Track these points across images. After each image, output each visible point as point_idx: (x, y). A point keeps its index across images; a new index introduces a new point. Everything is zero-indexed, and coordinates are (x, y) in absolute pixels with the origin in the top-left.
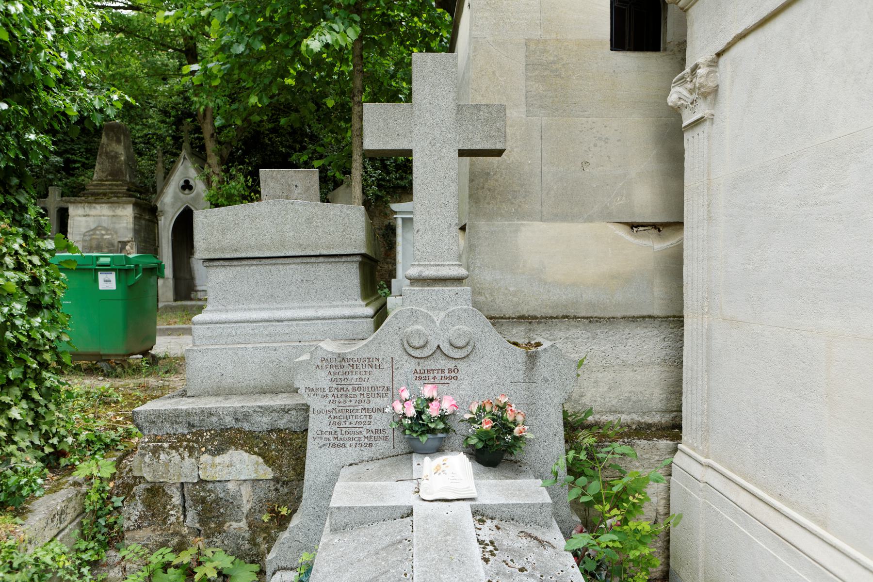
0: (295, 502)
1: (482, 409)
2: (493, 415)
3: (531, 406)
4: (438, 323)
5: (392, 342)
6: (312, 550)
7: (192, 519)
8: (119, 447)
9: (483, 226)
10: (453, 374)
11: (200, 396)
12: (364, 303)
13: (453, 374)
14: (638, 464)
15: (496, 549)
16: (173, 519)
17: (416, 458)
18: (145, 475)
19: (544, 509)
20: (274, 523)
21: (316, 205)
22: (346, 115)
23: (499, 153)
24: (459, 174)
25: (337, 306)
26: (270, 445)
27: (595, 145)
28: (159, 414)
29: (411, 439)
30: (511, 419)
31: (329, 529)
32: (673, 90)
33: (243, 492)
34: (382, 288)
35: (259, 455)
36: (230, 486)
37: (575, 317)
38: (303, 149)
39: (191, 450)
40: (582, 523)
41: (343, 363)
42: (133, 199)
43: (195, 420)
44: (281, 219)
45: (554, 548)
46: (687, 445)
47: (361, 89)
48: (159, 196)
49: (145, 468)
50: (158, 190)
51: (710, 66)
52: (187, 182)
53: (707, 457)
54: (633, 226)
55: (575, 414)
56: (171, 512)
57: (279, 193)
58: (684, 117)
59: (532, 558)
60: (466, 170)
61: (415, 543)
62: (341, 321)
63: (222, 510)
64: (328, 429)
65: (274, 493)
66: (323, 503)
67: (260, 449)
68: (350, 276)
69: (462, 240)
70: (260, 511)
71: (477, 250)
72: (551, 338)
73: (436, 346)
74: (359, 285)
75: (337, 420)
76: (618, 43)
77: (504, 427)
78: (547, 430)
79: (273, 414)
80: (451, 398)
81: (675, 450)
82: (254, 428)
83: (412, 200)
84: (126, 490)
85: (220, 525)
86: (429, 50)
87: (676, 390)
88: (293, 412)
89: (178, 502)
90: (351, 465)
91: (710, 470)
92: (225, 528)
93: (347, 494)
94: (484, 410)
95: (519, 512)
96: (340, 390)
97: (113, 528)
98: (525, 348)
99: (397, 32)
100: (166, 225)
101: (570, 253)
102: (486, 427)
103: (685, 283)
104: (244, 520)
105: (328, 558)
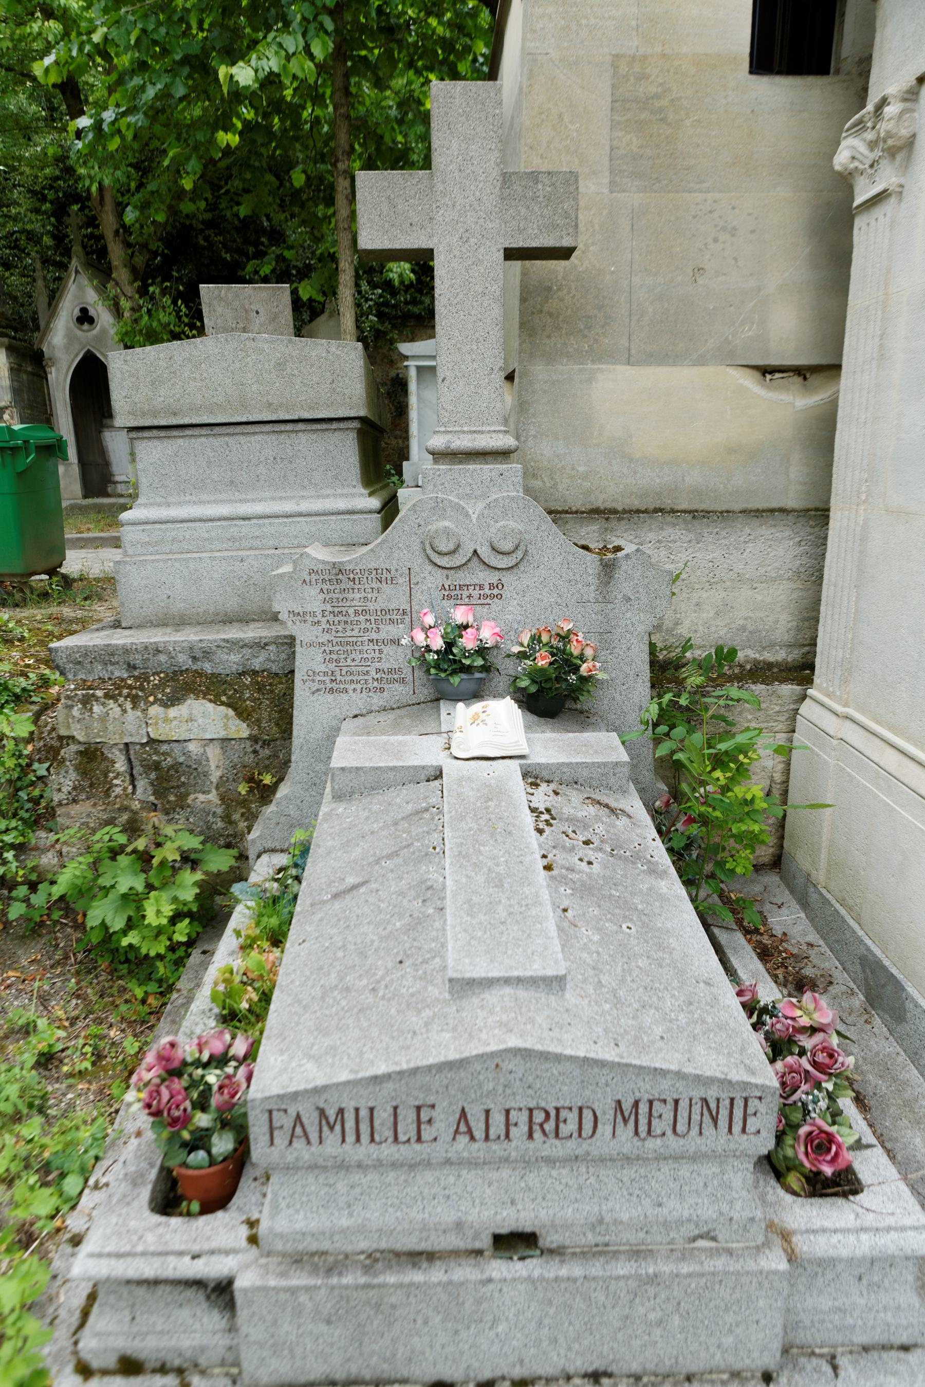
0: (282, 768)
1: (536, 639)
2: (552, 647)
3: (605, 638)
4: (474, 518)
5: (408, 546)
6: (309, 827)
7: (144, 790)
8: (34, 699)
9: (540, 371)
10: (496, 592)
11: (140, 627)
12: (366, 492)
13: (496, 592)
14: (750, 717)
15: (554, 819)
16: (118, 790)
17: (444, 706)
18: (75, 733)
19: (618, 770)
20: (254, 795)
21: (290, 341)
22: (325, 196)
23: (565, 253)
24: (504, 289)
25: (328, 496)
26: (242, 693)
27: (716, 240)
28: (86, 652)
29: (438, 680)
30: (576, 652)
31: (330, 797)
32: (844, 144)
33: (210, 755)
34: (389, 475)
35: (228, 705)
36: (192, 747)
37: (673, 511)
38: (260, 255)
39: (135, 700)
40: (670, 792)
41: (340, 576)
42: (6, 340)
43: (137, 659)
44: (238, 365)
45: (629, 816)
46: (819, 690)
47: (347, 148)
48: (44, 334)
49: (74, 723)
50: (42, 324)
51: (905, 100)
52: (84, 311)
53: (846, 705)
54: (765, 371)
55: (666, 648)
56: (115, 782)
57: (231, 323)
58: (857, 189)
59: (600, 829)
60: (516, 282)
61: (446, 809)
62: (334, 517)
63: (183, 779)
64: (323, 668)
65: (252, 756)
66: (320, 767)
67: (229, 698)
68: (345, 450)
69: (508, 397)
70: (234, 780)
71: (532, 410)
72: (636, 540)
73: (472, 550)
74: (358, 465)
75: (334, 657)
76: (767, 57)
77: (566, 663)
78: (627, 669)
79: (244, 651)
80: (493, 623)
81: (804, 697)
82: (219, 670)
83: (433, 336)
84: (51, 754)
85: (183, 797)
86: (455, 76)
87: (810, 616)
88: (272, 648)
89: (123, 769)
90: (356, 716)
91: (848, 723)
92: (189, 801)
93: (349, 751)
94: (540, 641)
95: (585, 773)
96: (337, 613)
97: (38, 804)
98: (599, 554)
99: (400, 43)
100: (60, 380)
101: (670, 412)
102: (541, 663)
103: (836, 459)
104: (214, 791)
105: (331, 831)
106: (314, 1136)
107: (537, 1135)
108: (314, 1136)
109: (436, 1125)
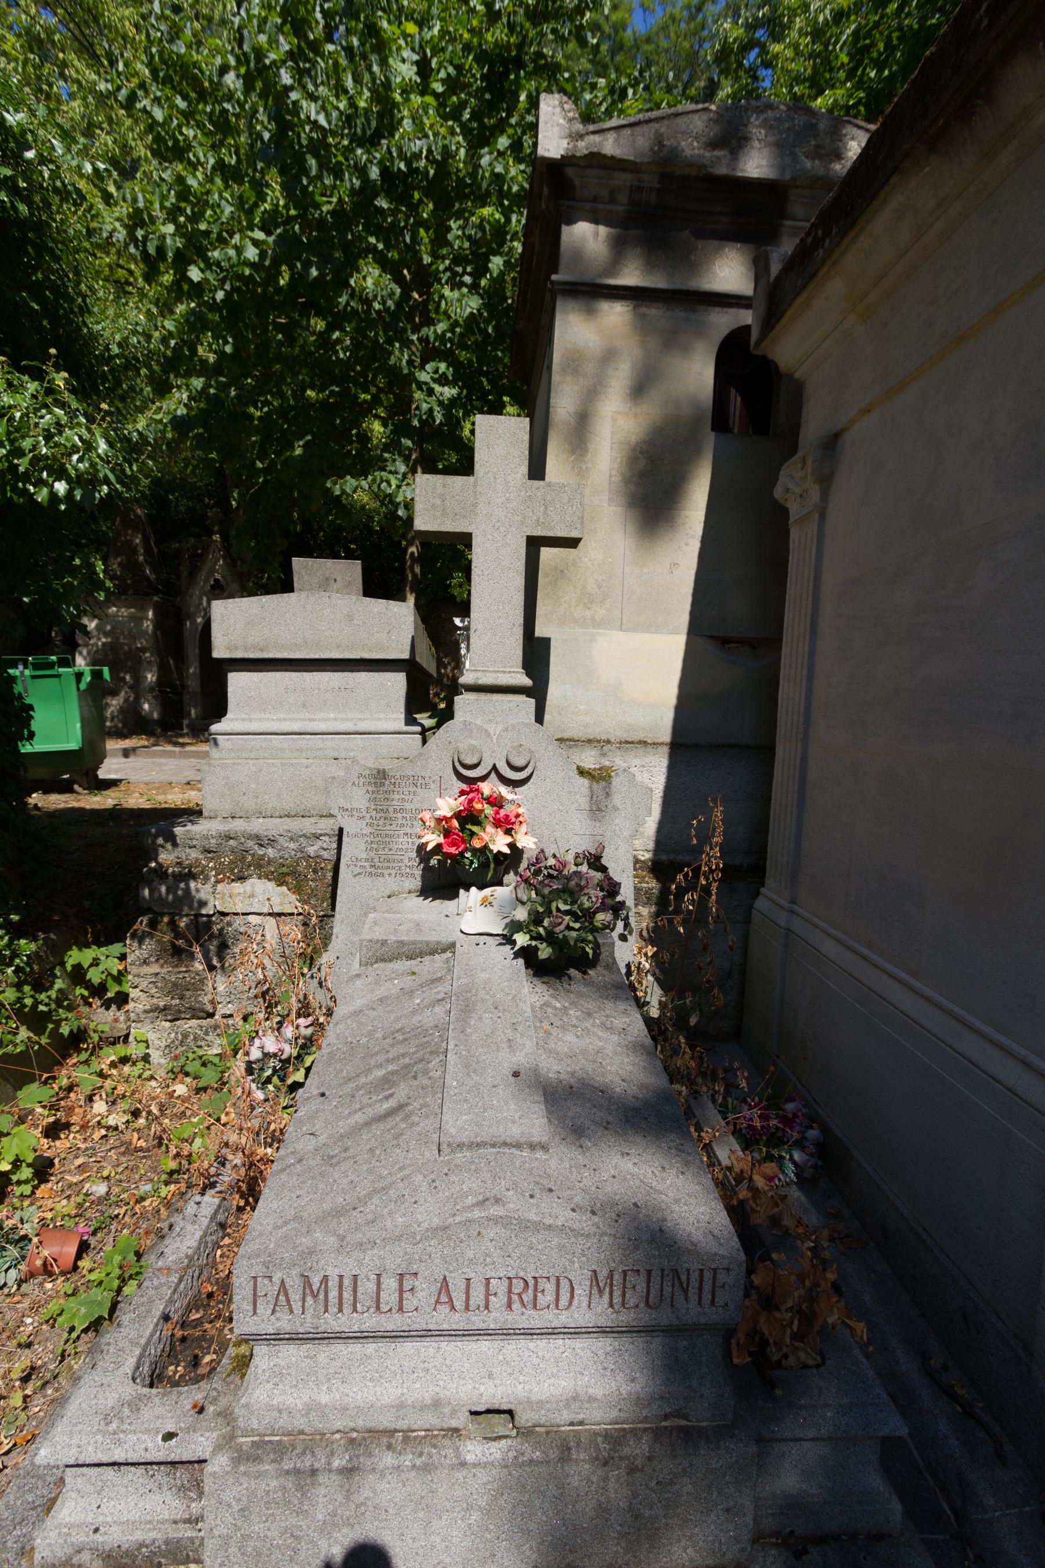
23: (572, 543)
106: (297, 1306)
107: (516, 1306)
108: (297, 1306)
109: (420, 1294)
